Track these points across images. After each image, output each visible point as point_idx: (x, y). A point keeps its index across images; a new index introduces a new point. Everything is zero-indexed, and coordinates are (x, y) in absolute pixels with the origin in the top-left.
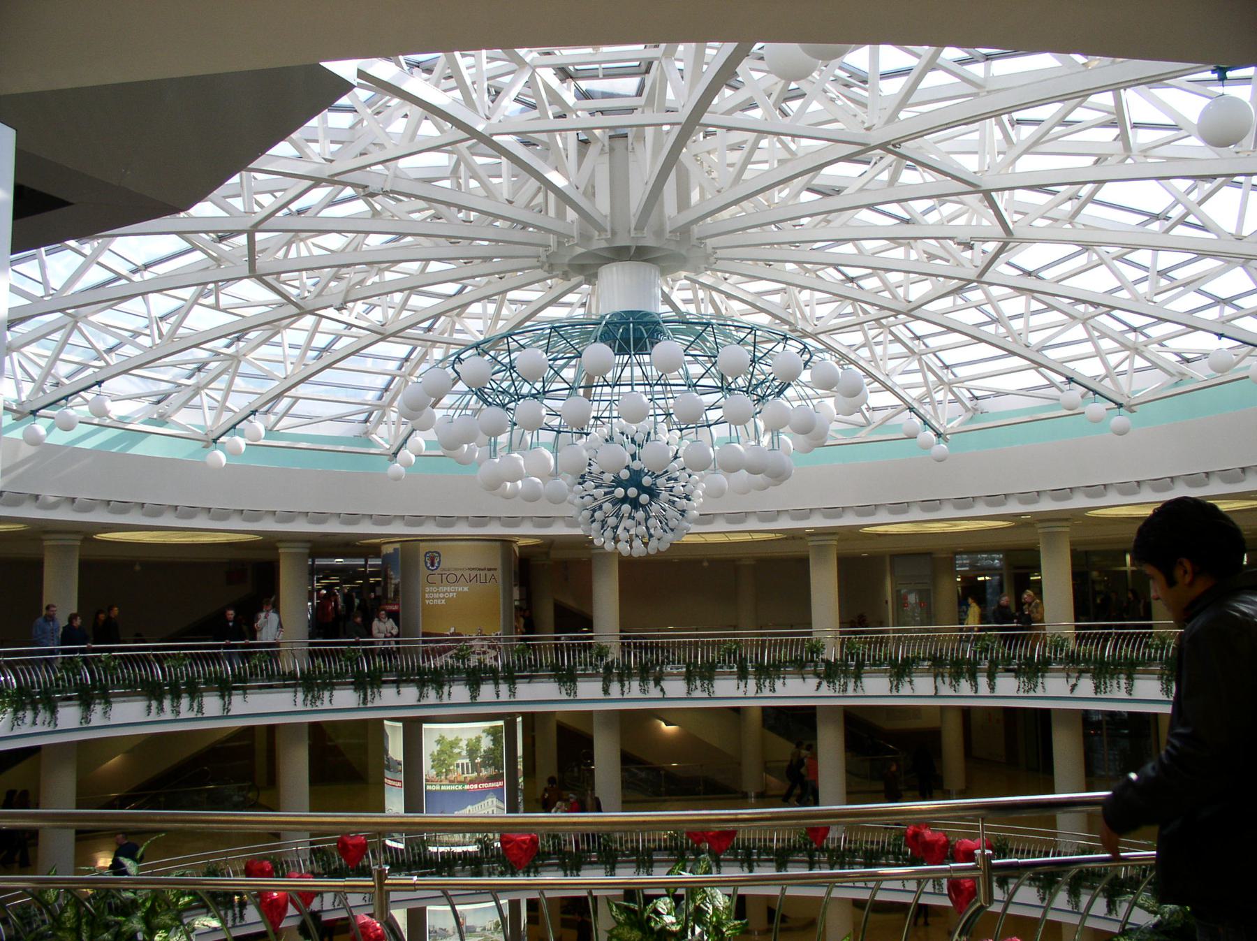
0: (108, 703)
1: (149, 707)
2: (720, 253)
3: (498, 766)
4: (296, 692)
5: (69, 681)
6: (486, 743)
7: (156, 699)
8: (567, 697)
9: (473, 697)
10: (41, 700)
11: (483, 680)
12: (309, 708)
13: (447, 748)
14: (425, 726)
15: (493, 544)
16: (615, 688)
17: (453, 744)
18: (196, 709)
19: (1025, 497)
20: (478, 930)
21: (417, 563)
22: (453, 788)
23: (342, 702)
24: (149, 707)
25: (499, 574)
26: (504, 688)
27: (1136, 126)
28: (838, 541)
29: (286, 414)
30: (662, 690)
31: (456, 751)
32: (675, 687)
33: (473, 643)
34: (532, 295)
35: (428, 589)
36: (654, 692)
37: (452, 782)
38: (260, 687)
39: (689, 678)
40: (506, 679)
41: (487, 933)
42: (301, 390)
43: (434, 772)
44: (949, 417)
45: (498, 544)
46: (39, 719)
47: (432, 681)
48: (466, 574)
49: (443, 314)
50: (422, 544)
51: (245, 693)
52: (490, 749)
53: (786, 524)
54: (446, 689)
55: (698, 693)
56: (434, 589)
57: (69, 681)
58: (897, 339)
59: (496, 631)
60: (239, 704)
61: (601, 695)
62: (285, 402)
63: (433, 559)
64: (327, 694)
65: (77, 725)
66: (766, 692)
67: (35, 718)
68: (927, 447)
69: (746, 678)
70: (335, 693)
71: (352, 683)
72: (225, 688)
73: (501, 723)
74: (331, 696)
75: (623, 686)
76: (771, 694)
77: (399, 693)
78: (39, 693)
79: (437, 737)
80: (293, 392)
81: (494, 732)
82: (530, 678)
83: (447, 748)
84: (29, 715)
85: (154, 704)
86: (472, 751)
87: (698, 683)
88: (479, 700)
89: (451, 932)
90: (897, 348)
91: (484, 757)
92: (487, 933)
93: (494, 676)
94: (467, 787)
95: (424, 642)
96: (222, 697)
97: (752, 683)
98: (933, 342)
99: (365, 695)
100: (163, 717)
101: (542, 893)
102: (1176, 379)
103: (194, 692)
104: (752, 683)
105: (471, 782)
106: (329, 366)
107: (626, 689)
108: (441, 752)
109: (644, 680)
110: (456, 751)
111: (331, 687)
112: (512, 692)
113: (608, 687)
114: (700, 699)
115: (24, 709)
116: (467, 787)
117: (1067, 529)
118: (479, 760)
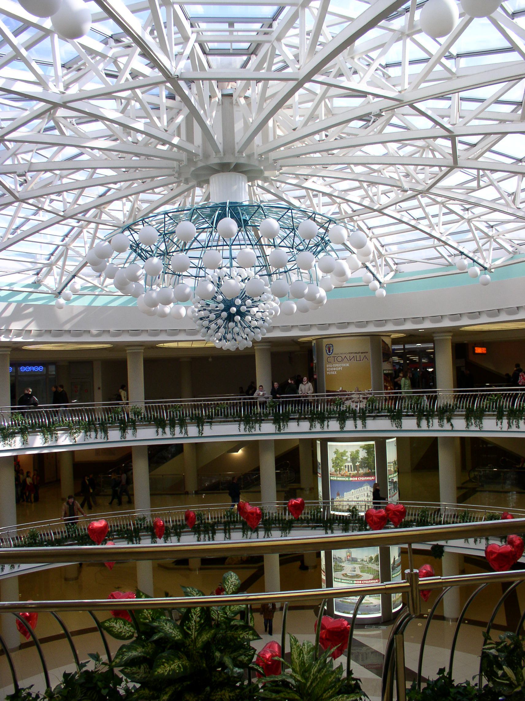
0: (135, 429)
1: (157, 431)
3: (370, 467)
4: (240, 425)
5: (115, 418)
6: (363, 454)
7: (161, 427)
8: (396, 429)
9: (342, 428)
10: (178, 423)
11: (348, 418)
12: (248, 433)
13: (340, 456)
14: (329, 443)
15: (364, 337)
16: (424, 423)
17: (343, 454)
18: (184, 433)
19: (415, 320)
20: (359, 560)
21: (322, 350)
22: (343, 479)
23: (298, 429)
24: (157, 431)
25: (369, 356)
26: (359, 422)
27: (61, 201)
28: (452, 336)
30: (452, 425)
31: (345, 458)
32: (459, 423)
33: (353, 396)
35: (328, 366)
36: (447, 426)
37: (343, 476)
38: (221, 422)
39: (467, 418)
40: (360, 418)
41: (364, 563)
43: (333, 470)
45: (369, 337)
46: (99, 436)
47: (318, 418)
48: (348, 356)
50: (324, 340)
51: (211, 425)
52: (365, 458)
54: (326, 423)
55: (473, 428)
56: (331, 365)
57: (115, 418)
59: (369, 390)
60: (207, 430)
61: (416, 428)
63: (330, 348)
64: (257, 425)
65: (119, 440)
66: (514, 428)
67: (96, 435)
69: (502, 419)
70: (262, 425)
71: (271, 420)
72: (199, 422)
73: (373, 443)
74: (260, 426)
75: (428, 422)
76: (517, 430)
77: (298, 424)
78: (178, 420)
79: (334, 450)
81: (368, 449)
82: (374, 417)
83: (339, 456)
84: (93, 434)
85: (160, 430)
86: (354, 459)
87: (473, 421)
88: (345, 429)
89: (344, 560)
91: (361, 462)
92: (364, 563)
93: (354, 415)
94: (351, 479)
95: (328, 396)
96: (198, 426)
97: (505, 421)
99: (280, 426)
100: (165, 436)
101: (410, 545)
102: (511, 255)
103: (183, 424)
104: (505, 421)
105: (354, 476)
107: (430, 424)
108: (337, 458)
109: (441, 419)
110: (345, 458)
111: (260, 421)
112: (364, 425)
113: (420, 422)
114: (473, 432)
115: (90, 431)
116: (351, 479)
118: (358, 464)
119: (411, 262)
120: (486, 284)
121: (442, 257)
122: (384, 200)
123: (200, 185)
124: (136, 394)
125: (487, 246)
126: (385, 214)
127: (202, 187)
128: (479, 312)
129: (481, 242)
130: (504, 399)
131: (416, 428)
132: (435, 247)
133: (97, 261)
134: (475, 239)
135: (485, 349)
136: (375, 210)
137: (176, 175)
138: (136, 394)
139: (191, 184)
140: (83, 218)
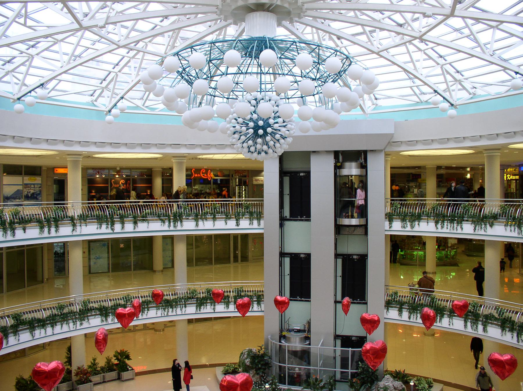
2: (309, 13)
29: (53, 89)
34: (202, 28)
42: (64, 76)
44: (460, 96)
49: (141, 40)
53: (62, 148)
58: (430, 58)
61: (472, 232)
62: (54, 82)
68: (444, 110)
80: (59, 78)
90: (431, 63)
98: (449, 59)
102: (471, 96)
106: (80, 64)
117: (500, 154)
119: (389, 97)
120: (452, 117)
121: (416, 94)
122: (386, 43)
123: (235, 23)
124: (76, 200)
125: (454, 87)
126: (381, 56)
127: (237, 25)
128: (497, 134)
129: (450, 84)
130: (473, 208)
131: (472, 232)
132: (411, 87)
133: (149, 83)
134: (446, 82)
135: (255, 183)
136: (373, 52)
137: (218, 12)
138: (76, 200)
139: (229, 21)
140: (134, 48)
